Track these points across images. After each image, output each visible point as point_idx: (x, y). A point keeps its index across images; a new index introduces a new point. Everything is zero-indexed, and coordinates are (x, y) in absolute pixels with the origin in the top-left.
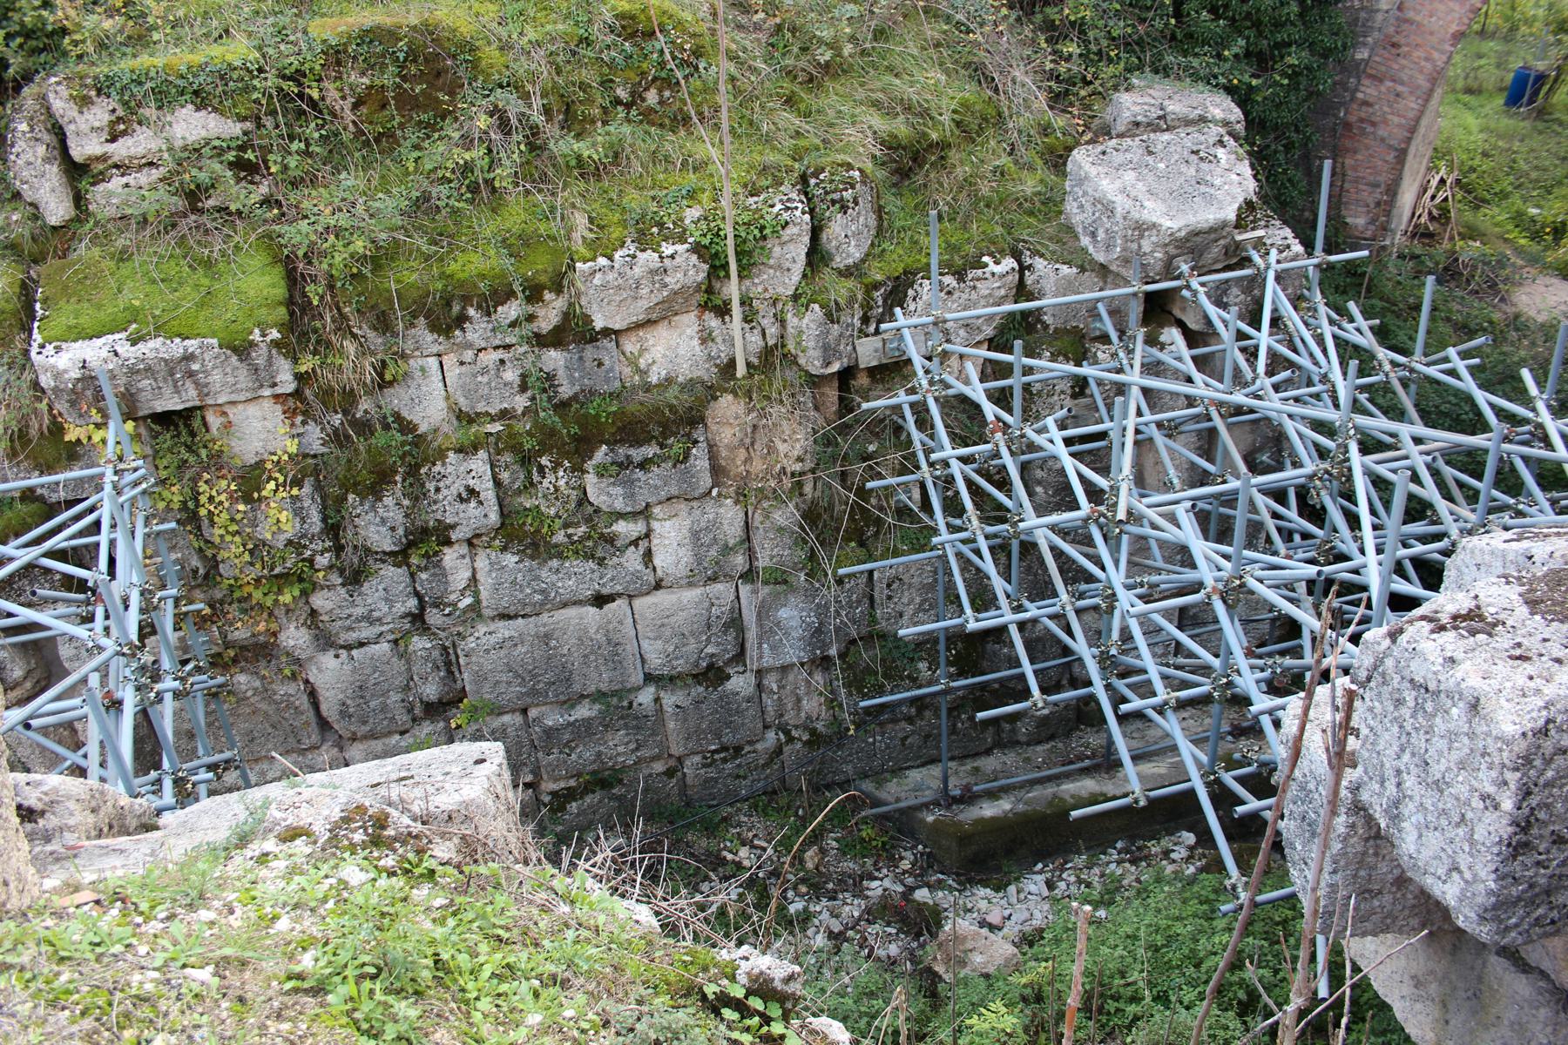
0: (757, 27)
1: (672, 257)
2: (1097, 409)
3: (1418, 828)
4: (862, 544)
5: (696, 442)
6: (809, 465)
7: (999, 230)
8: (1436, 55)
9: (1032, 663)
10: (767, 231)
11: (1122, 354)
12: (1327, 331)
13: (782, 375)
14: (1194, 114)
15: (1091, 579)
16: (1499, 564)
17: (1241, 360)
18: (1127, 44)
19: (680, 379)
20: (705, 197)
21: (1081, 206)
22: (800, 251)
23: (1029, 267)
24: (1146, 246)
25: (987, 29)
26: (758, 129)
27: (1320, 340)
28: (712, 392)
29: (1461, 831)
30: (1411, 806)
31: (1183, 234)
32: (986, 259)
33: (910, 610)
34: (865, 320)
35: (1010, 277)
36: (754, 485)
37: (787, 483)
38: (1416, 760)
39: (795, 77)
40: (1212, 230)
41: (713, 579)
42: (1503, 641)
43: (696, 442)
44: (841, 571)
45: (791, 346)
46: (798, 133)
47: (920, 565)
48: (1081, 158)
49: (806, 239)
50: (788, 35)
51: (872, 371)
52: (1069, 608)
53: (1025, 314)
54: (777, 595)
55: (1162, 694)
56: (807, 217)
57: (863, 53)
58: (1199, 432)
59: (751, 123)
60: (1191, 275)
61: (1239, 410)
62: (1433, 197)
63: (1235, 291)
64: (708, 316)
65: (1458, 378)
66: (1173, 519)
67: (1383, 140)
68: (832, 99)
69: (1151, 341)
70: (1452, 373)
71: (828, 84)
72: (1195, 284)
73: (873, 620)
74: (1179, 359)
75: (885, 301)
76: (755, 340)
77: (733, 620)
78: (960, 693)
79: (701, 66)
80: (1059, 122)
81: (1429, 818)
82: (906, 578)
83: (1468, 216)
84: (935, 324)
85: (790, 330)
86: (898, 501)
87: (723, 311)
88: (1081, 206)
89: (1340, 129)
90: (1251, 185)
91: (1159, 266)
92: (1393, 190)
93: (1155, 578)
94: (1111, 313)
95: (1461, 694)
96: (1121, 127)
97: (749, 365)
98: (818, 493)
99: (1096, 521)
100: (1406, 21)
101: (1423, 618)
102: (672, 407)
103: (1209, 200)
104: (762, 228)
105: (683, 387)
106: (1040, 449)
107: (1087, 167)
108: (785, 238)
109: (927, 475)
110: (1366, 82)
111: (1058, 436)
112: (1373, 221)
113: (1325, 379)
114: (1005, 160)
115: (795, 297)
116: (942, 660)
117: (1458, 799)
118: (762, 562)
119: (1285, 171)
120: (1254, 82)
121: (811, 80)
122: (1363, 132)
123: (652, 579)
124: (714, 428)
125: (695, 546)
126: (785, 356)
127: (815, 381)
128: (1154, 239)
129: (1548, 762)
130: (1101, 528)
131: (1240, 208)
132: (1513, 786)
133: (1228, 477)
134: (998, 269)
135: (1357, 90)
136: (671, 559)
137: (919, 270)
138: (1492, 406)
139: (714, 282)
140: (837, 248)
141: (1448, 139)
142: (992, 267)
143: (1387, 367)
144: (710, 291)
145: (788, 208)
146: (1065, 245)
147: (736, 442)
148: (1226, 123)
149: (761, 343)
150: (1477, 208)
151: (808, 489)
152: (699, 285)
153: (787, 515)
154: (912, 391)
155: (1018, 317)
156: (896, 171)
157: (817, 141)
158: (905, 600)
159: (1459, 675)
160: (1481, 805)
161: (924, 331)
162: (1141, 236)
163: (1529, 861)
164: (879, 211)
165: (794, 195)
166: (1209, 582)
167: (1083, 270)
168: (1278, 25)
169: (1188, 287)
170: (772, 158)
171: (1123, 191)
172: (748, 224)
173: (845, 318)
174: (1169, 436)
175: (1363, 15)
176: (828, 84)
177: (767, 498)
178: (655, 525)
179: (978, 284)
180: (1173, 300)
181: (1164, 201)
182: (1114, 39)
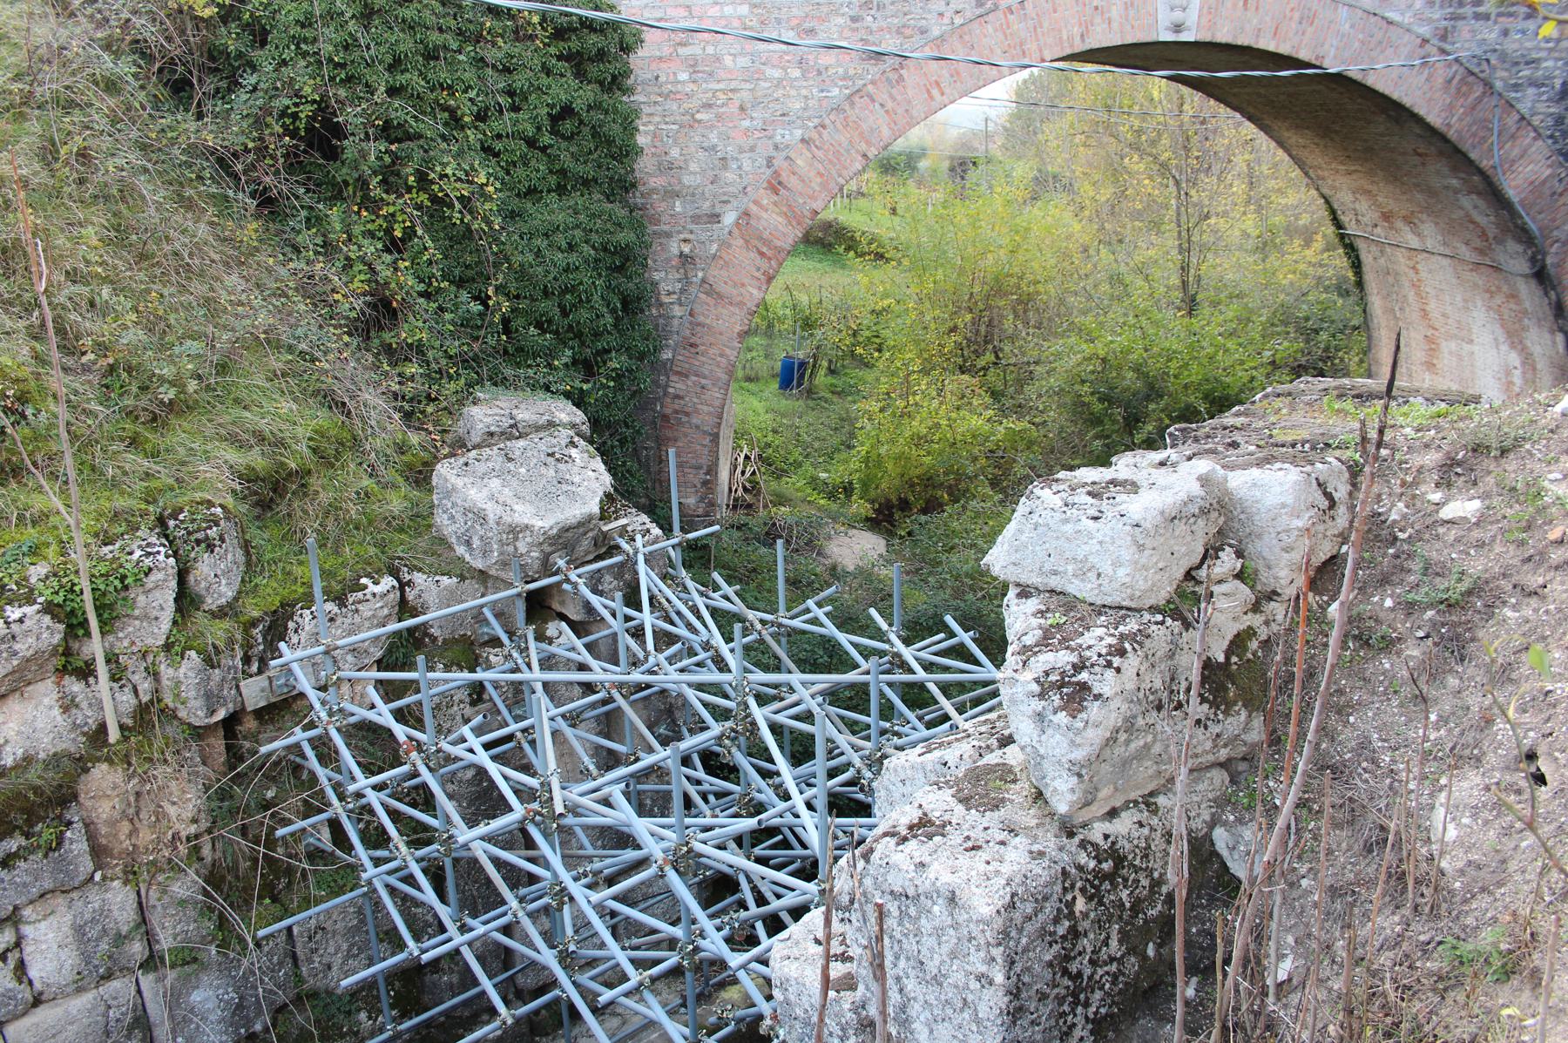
0: (86, 369)
1: (21, 621)
2: (499, 712)
3: (928, 1025)
4: (275, 900)
5: (69, 824)
6: (204, 825)
7: (372, 551)
8: (728, 351)
9: (490, 978)
10: (129, 581)
11: (515, 655)
12: (700, 602)
13: (161, 733)
14: (543, 420)
15: (533, 879)
16: (921, 775)
17: (631, 642)
18: (465, 361)
19: (42, 755)
20: (52, 551)
21: (452, 517)
22: (167, 597)
23: (409, 583)
24: (522, 547)
25: (331, 357)
26: (102, 474)
27: (695, 611)
28: (82, 764)
29: (966, 1015)
30: (917, 1006)
31: (555, 531)
32: (364, 581)
33: (338, 960)
34: (247, 660)
35: (392, 596)
36: (145, 859)
37: (183, 849)
38: (912, 963)
39: (137, 418)
40: (580, 524)
41: (108, 977)
42: (955, 838)
43: (69, 824)
44: (261, 933)
45: (168, 700)
46: (147, 474)
47: (343, 909)
48: (445, 472)
49: (173, 584)
50: (124, 375)
51: (259, 713)
52: (521, 914)
53: (411, 631)
54: (186, 978)
55: (635, 977)
56: (172, 561)
57: (208, 388)
58: (597, 718)
59: (93, 469)
60: (569, 569)
61: (640, 687)
62: (743, 473)
63: (608, 578)
64: (67, 680)
65: (822, 625)
66: (606, 802)
67: (697, 427)
68: (180, 436)
69: (540, 637)
70: (815, 621)
71: (173, 421)
72: (573, 576)
73: (300, 979)
74: (573, 649)
75: (264, 638)
76: (127, 700)
77: (136, 1020)
78: (406, 1036)
79: (29, 412)
80: (414, 438)
81: (936, 1012)
82: (328, 925)
83: (774, 485)
84: (326, 653)
85: (165, 682)
86: (308, 845)
87: (86, 672)
88: (452, 517)
89: (659, 422)
90: (607, 479)
91: (537, 565)
92: (712, 470)
93: (597, 865)
94: (497, 616)
95: (938, 892)
96: (476, 438)
97: (122, 727)
98: (219, 854)
99: (533, 820)
100: (699, 324)
101: (886, 834)
102: (37, 790)
103: (573, 497)
104: (123, 578)
105: (47, 764)
106: (457, 759)
107: (453, 479)
108: (150, 585)
109: (340, 811)
110: (674, 378)
111: (475, 742)
112: (702, 500)
113: (707, 646)
114: (367, 482)
115: (168, 647)
116: (385, 1005)
117: (956, 987)
118: (165, 942)
119: (624, 463)
120: (585, 387)
121: (154, 419)
122: (680, 423)
123: (29, 996)
124: (88, 804)
125: (80, 942)
126: (162, 711)
127: (199, 733)
128: (528, 539)
129: (1020, 930)
130: (537, 825)
131: (601, 501)
132: (999, 960)
133: (641, 754)
134: (377, 589)
135: (667, 386)
136: (51, 966)
137: (297, 601)
138: (855, 645)
139: (71, 643)
140: (207, 589)
141: (743, 422)
142: (372, 588)
143: (759, 626)
144: (67, 653)
145: (149, 554)
146: (441, 557)
147: (116, 815)
148: (573, 426)
149: (134, 701)
150: (779, 478)
151: (206, 851)
152: (55, 648)
153: (187, 885)
154: (311, 726)
155: (405, 634)
156: (257, 504)
157: (171, 481)
158: (331, 950)
159: (932, 876)
160: (978, 985)
161: (312, 664)
162: (516, 539)
163: (1025, 1023)
164: (246, 546)
165: (153, 540)
166: (659, 855)
167: (462, 578)
168: (597, 335)
169: (568, 580)
170: (121, 503)
171: (492, 497)
172: (107, 575)
173: (226, 661)
174: (573, 726)
175: (661, 321)
176: (173, 421)
177: (162, 870)
178: (27, 930)
179: (360, 607)
180: (551, 596)
181: (531, 502)
182: (451, 357)
